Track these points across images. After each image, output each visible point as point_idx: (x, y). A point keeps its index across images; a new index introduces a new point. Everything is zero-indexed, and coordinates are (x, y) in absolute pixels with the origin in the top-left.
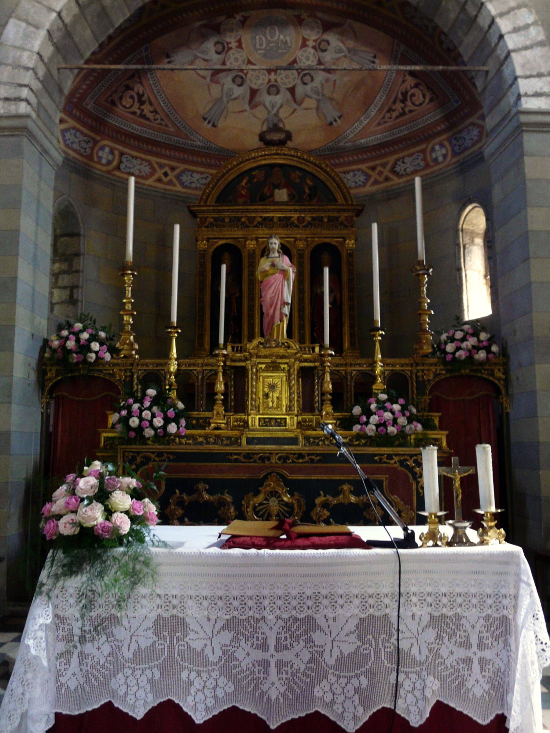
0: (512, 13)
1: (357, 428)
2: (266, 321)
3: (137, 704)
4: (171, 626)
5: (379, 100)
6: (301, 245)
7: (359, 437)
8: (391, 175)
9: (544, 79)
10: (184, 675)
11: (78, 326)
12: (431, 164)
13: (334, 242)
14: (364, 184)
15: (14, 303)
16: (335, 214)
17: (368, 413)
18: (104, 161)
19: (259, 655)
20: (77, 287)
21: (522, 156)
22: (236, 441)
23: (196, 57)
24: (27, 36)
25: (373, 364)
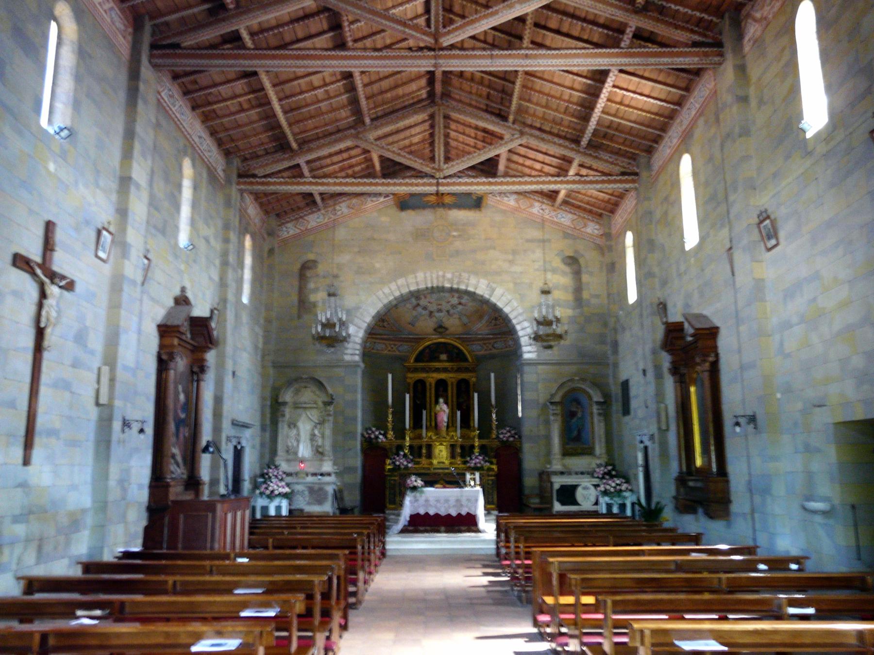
4: (427, 501)
5: (486, 318)
6: (453, 380)
11: (374, 429)
17: (471, 459)
24: (357, 332)
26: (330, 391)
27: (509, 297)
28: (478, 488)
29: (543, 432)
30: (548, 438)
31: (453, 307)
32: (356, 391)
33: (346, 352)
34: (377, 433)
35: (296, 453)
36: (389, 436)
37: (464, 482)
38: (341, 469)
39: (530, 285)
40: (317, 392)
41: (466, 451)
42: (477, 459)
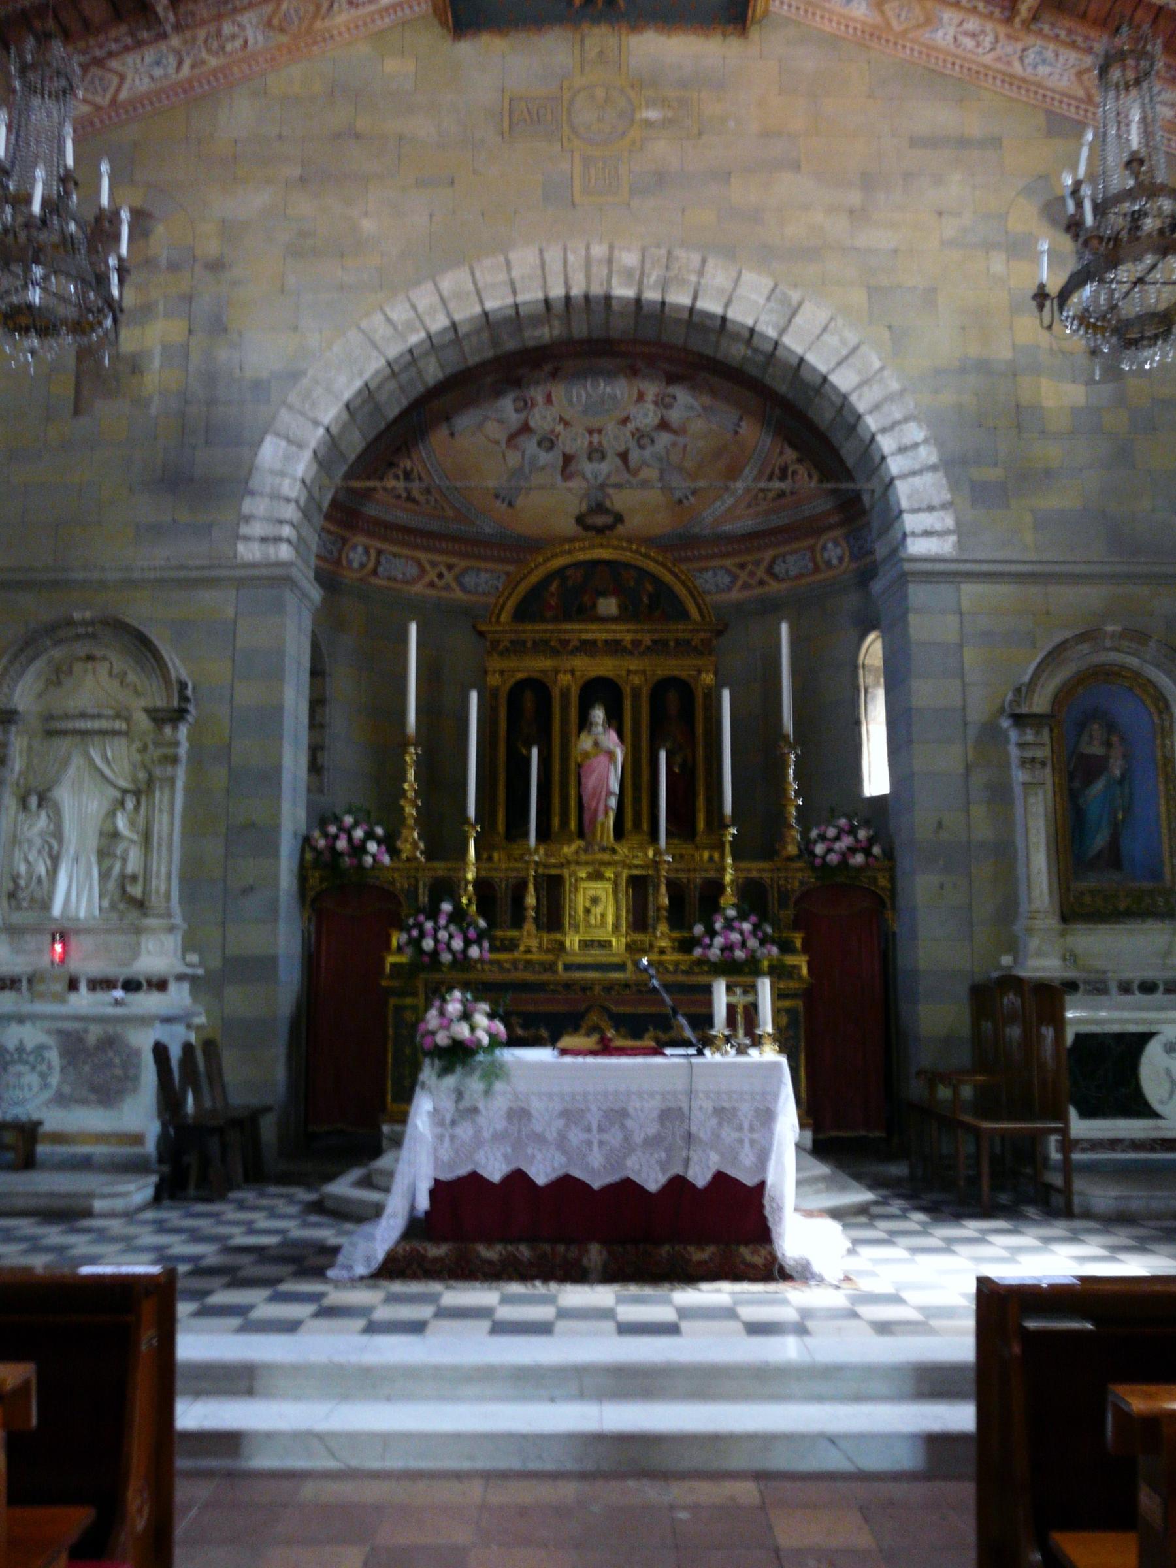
0: (897, 429)
1: (698, 952)
2: (587, 817)
3: (495, 1171)
4: (518, 1114)
6: (636, 680)
7: (700, 962)
8: (766, 578)
9: (935, 514)
10: (529, 1151)
11: (349, 820)
12: (822, 566)
13: (684, 675)
14: (729, 589)
15: (278, 798)
16: (687, 636)
17: (712, 933)
18: (356, 565)
19: (586, 1136)
20: (322, 748)
21: (906, 612)
22: (550, 967)
23: (486, 418)
24: (287, 458)
25: (722, 870)
26: (178, 668)
27: (852, 337)
28: (770, 1054)
29: (983, 831)
30: (1004, 853)
31: (641, 438)
32: (276, 675)
33: (244, 530)
34: (359, 834)
35: (45, 905)
36: (406, 849)
37: (703, 1021)
38: (216, 963)
39: (929, 297)
40: (132, 677)
41: (693, 904)
42: (733, 934)
